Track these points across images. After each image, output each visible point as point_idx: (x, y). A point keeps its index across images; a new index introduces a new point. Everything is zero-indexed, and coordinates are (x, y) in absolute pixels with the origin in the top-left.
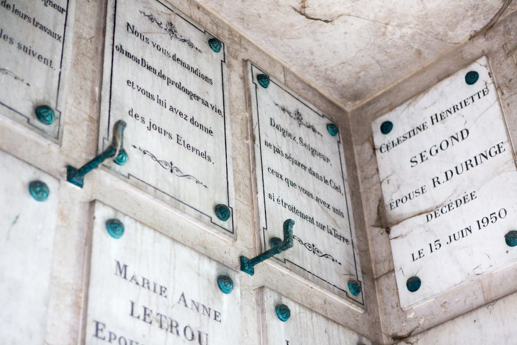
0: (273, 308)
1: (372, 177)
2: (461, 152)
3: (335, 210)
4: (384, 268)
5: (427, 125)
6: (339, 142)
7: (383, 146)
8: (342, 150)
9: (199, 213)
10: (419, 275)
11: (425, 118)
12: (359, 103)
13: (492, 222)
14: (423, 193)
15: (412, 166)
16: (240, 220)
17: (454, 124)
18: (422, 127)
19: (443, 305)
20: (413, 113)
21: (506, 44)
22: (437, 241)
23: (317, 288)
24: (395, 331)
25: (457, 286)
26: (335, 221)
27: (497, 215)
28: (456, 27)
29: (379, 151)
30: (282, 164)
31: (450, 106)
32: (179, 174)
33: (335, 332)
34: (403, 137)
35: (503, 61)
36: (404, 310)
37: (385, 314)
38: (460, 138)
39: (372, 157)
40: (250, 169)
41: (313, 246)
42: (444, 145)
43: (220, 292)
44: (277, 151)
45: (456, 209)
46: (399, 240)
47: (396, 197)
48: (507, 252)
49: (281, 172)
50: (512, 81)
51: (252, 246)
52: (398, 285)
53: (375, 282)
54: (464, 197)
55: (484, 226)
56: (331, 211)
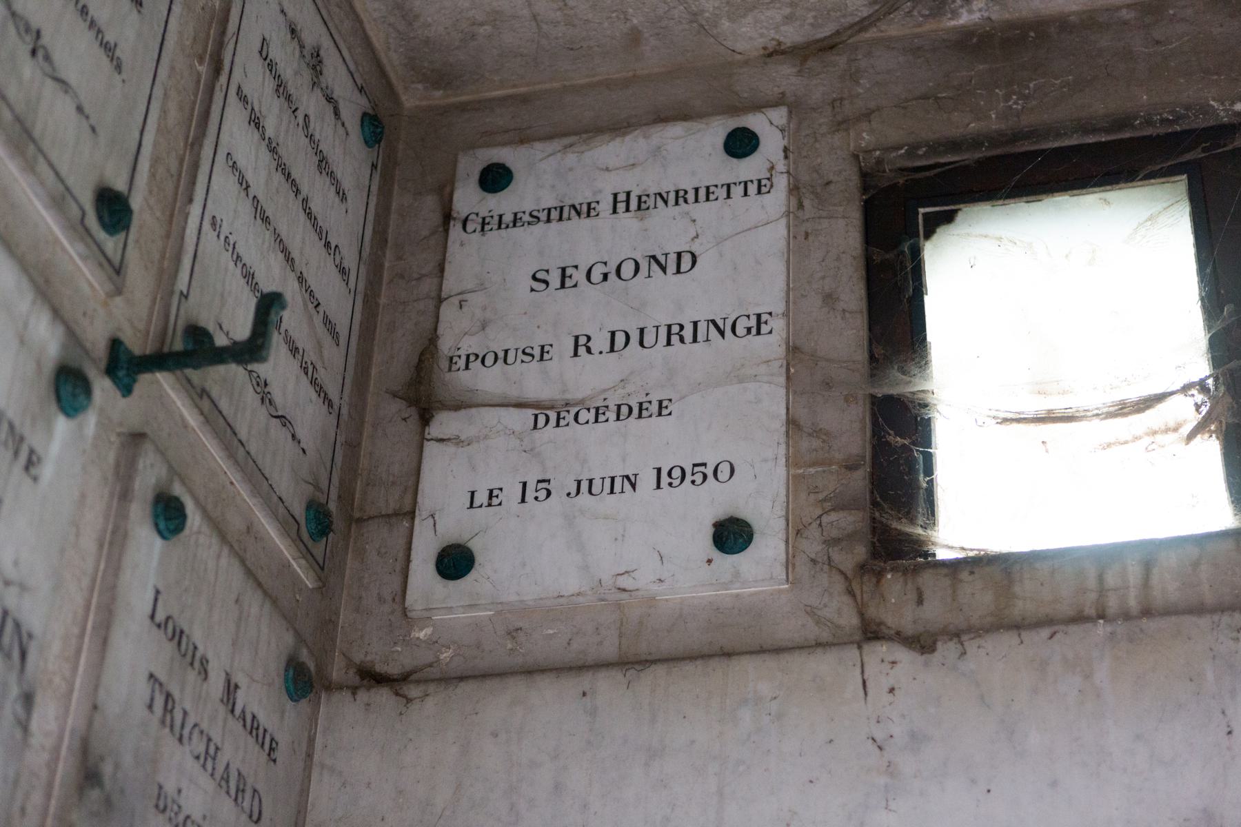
0: (150, 496)
1: (418, 279)
2: (664, 299)
3: (327, 321)
4: (386, 500)
5: (599, 208)
6: (374, 166)
7: (473, 217)
8: (374, 188)
9: (61, 188)
10: (475, 546)
11: (600, 191)
12: (438, 97)
13: (693, 482)
14: (542, 359)
15: (532, 290)
16: (139, 246)
17: (668, 230)
18: (585, 208)
19: (513, 633)
20: (571, 169)
21: (842, 99)
22: (544, 481)
23: (243, 491)
24: (369, 658)
25: (561, 600)
26: (319, 345)
27: (709, 471)
28: (744, 16)
29: (459, 226)
30: (257, 157)
31: (667, 186)
32: (48, 69)
33: (255, 610)
34: (531, 215)
35: (823, 135)
36: (409, 614)
37: (357, 610)
38: (671, 268)
39: (433, 233)
40: (188, 137)
41: (266, 385)
42: (628, 270)
43: (54, 407)
44: (256, 122)
45: (612, 423)
46: (450, 449)
47: (470, 345)
48: (709, 561)
49: (250, 177)
50: (832, 187)
51: (141, 326)
52: (413, 553)
53: (354, 526)
54: (641, 404)
55: (670, 484)
56: (318, 320)
